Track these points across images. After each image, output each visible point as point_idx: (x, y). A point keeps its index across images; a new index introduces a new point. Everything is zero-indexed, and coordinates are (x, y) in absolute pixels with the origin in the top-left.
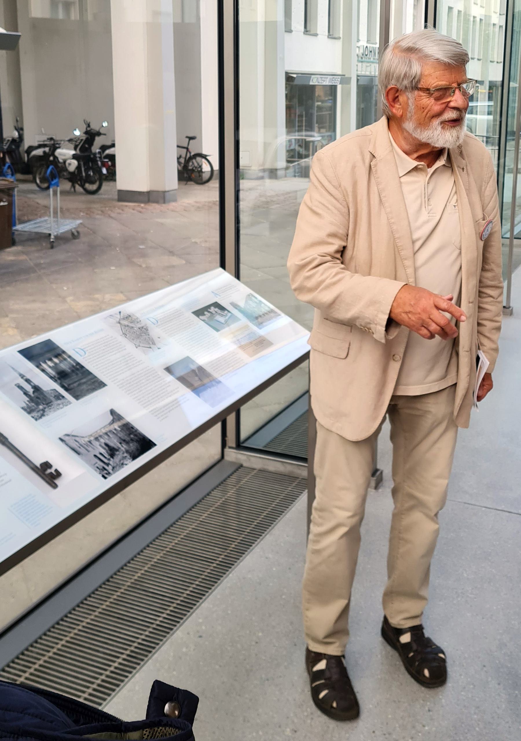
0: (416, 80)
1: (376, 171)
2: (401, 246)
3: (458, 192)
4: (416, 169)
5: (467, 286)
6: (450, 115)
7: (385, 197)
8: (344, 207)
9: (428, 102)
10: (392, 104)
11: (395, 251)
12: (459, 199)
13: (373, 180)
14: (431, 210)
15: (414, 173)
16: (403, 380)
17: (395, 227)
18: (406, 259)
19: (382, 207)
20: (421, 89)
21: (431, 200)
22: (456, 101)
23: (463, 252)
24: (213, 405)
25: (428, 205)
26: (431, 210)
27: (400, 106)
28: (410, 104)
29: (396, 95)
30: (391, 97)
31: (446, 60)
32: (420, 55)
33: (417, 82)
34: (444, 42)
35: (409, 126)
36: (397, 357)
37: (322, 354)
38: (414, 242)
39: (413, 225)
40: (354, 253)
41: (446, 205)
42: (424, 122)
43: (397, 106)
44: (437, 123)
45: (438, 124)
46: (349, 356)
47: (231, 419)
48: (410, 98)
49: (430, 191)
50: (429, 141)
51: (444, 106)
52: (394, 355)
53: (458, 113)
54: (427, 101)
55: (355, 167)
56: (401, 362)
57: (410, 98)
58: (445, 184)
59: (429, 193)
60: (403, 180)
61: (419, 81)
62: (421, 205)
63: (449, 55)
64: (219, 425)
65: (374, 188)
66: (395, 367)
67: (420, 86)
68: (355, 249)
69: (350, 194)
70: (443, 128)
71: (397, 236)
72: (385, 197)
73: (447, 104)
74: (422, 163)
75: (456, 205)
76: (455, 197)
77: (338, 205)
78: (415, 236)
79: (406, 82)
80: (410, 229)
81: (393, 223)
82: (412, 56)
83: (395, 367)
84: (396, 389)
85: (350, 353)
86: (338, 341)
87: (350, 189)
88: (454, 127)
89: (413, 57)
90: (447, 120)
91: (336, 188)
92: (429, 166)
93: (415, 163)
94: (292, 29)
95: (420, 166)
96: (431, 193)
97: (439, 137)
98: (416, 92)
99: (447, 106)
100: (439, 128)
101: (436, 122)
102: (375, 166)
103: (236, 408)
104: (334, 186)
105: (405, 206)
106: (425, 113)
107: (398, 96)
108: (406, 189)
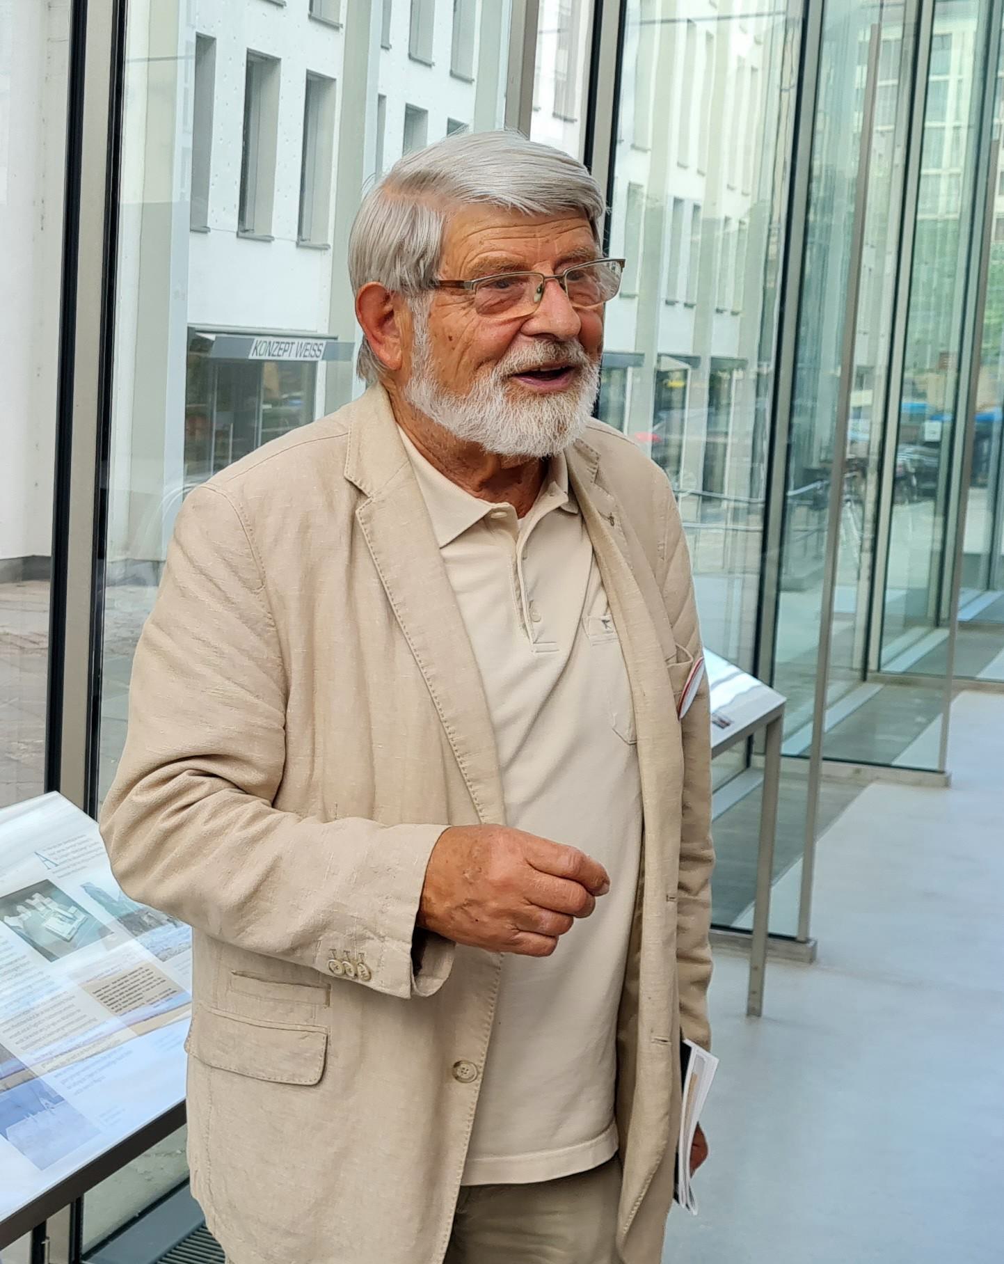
0: (429, 256)
1: (372, 532)
2: (462, 743)
3: (608, 582)
4: (486, 523)
5: (662, 852)
6: (529, 353)
7: (403, 604)
8: (268, 643)
9: (464, 322)
10: (378, 334)
11: (443, 757)
12: (614, 600)
13: (362, 560)
14: (541, 633)
15: (485, 535)
16: (486, 1143)
17: (439, 690)
18: (476, 781)
19: (397, 634)
20: (442, 285)
21: (536, 605)
22: (545, 314)
23: (644, 749)
24: (42, 1164)
25: (532, 620)
26: (541, 633)
27: (397, 341)
28: (418, 332)
29: (388, 308)
30: (371, 315)
31: (510, 199)
32: (442, 191)
33: (431, 264)
34: (518, 157)
35: (420, 392)
36: (467, 1070)
37: (237, 1079)
38: (496, 730)
39: (493, 682)
40: (317, 772)
41: (581, 619)
42: (453, 385)
43: (390, 339)
44: (492, 381)
45: (495, 384)
46: (328, 1074)
47: (57, 1225)
48: (419, 313)
49: (530, 580)
50: (477, 437)
51: (509, 329)
52: (457, 1064)
53: (551, 349)
54: (461, 317)
55: (308, 527)
56: (479, 1082)
57: (419, 313)
58: (567, 561)
59: (529, 587)
60: (447, 552)
61: (435, 264)
62: (510, 620)
63: (514, 188)
64: (26, 1240)
65: (367, 584)
66: (464, 1095)
67: (440, 277)
68: (319, 761)
69: (293, 606)
70: (511, 397)
71: (447, 714)
72: (403, 604)
73: (518, 323)
74: (505, 505)
75: (607, 617)
76: (602, 599)
77: (253, 640)
78: (500, 713)
79: (401, 271)
80: (484, 692)
81: (434, 677)
82: (423, 198)
83: (464, 1095)
84: (468, 1167)
85: (329, 1067)
86: (289, 1028)
87: (292, 591)
88: (543, 395)
89: (427, 199)
90: (516, 370)
91: (251, 589)
92: (522, 511)
93: (482, 507)
94: (539, 452)
95: (499, 514)
96: (535, 584)
97: (513, 424)
98: (432, 295)
99: (519, 331)
100: (499, 396)
101: (489, 379)
102: (369, 518)
103: (70, 1193)
104: (244, 582)
105: (464, 626)
106: (456, 353)
107: (391, 314)
108: (460, 577)
